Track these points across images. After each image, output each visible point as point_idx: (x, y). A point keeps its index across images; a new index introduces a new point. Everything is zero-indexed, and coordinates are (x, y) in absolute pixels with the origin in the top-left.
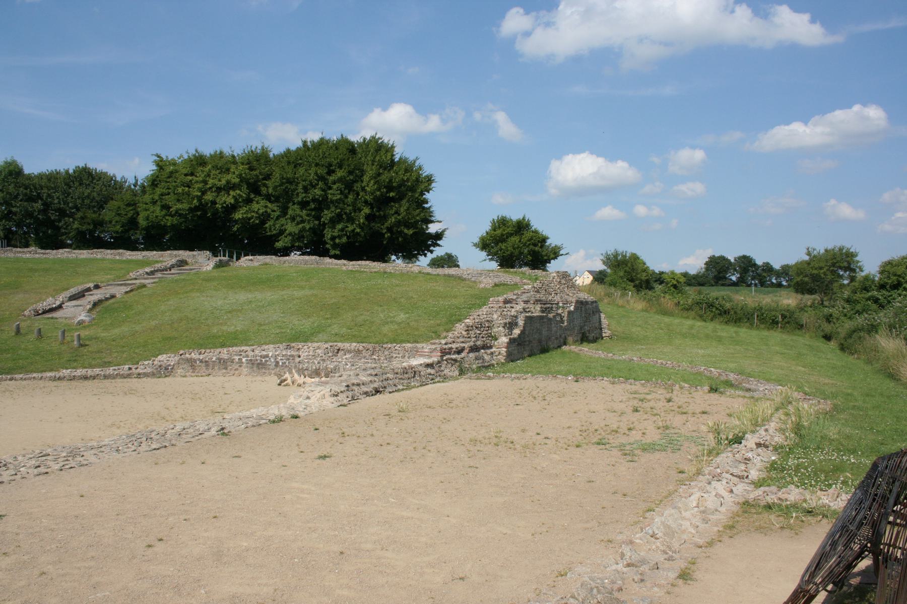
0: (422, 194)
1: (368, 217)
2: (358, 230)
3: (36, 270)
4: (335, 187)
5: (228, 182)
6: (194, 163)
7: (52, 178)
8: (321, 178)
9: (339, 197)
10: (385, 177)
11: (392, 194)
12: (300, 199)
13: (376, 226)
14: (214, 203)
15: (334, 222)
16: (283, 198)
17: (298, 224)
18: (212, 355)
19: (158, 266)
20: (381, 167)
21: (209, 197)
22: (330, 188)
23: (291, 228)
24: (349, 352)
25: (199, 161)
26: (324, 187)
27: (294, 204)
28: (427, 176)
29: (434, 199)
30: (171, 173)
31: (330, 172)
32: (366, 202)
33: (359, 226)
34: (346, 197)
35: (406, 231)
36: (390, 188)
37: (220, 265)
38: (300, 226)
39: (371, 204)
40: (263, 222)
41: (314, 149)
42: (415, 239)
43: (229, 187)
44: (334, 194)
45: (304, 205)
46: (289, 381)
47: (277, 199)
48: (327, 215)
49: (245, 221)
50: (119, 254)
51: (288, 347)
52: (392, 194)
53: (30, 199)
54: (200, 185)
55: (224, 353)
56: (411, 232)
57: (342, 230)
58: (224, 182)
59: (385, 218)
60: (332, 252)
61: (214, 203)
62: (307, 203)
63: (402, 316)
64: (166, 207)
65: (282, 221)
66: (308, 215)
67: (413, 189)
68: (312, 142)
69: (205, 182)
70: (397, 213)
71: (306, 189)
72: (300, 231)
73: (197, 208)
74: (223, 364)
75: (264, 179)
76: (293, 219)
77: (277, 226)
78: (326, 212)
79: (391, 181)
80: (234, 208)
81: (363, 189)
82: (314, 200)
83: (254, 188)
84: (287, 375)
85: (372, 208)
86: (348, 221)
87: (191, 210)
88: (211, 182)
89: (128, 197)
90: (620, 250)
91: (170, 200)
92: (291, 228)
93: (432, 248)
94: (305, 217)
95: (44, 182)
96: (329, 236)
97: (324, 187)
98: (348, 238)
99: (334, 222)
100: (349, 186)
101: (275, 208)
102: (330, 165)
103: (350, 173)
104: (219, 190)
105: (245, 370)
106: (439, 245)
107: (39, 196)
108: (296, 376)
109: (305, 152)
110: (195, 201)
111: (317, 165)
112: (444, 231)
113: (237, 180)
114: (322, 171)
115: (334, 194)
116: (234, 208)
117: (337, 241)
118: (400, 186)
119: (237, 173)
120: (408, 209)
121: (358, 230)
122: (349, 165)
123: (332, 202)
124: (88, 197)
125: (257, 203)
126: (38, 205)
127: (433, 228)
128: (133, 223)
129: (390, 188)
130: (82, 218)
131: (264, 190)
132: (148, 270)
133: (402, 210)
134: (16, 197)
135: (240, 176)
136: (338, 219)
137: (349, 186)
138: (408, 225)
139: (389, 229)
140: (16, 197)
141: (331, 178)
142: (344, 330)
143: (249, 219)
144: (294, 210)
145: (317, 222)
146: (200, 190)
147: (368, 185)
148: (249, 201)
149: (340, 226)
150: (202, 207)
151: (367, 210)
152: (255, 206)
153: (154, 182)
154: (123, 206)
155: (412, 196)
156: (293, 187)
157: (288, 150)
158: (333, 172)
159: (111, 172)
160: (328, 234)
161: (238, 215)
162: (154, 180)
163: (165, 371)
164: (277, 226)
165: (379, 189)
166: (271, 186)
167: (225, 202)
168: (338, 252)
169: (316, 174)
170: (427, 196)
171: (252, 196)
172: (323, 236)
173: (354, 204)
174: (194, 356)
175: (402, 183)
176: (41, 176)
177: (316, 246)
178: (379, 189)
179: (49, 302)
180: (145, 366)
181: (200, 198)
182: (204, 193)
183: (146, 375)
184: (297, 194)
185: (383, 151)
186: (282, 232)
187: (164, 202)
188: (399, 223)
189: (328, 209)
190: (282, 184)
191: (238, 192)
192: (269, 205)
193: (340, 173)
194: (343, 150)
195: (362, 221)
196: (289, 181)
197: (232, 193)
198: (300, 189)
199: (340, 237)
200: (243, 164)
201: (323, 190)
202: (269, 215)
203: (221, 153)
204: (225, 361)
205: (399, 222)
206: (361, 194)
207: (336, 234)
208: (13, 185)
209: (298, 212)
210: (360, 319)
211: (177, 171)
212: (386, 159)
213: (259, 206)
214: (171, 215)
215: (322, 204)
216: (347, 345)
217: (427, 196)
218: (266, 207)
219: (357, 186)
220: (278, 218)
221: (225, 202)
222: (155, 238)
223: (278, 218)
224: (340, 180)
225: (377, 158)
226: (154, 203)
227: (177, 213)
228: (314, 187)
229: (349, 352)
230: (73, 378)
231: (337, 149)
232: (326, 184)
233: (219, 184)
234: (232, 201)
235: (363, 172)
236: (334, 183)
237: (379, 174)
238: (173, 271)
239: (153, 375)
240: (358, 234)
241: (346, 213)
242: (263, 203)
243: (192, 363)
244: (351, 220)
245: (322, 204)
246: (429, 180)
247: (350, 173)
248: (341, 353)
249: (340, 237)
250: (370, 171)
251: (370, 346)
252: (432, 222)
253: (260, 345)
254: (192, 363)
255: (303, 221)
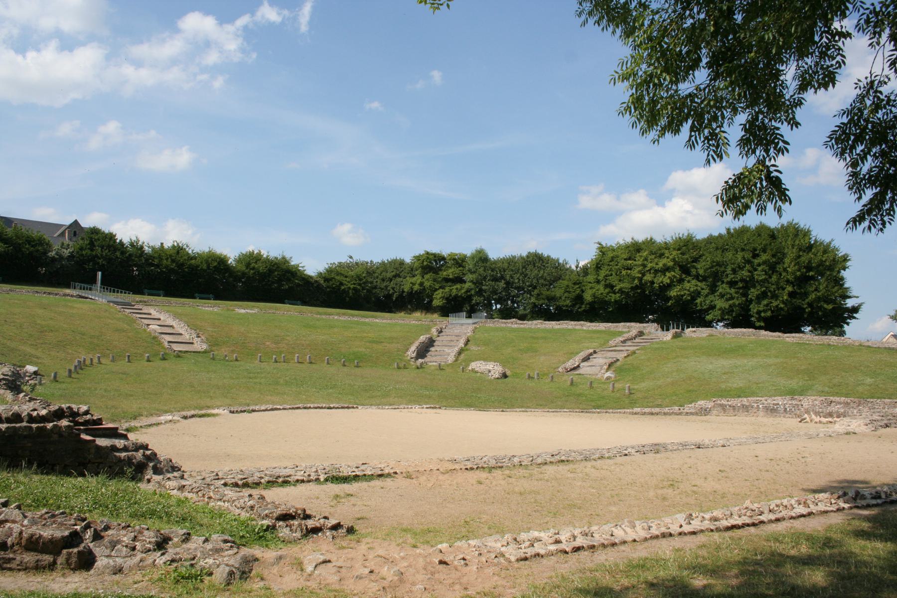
0: (839, 272)
1: (791, 295)
2: (782, 306)
3: (537, 338)
4: (760, 269)
5: (664, 265)
6: (632, 249)
7: (511, 262)
8: (748, 262)
9: (764, 277)
10: (805, 258)
11: (811, 273)
12: (729, 279)
13: (797, 302)
14: (652, 283)
15: (759, 299)
16: (714, 278)
17: (727, 300)
18: (737, 402)
19: (626, 336)
20: (800, 250)
21: (648, 277)
22: (756, 270)
23: (720, 304)
24: (840, 403)
25: (635, 248)
26: (751, 269)
27: (723, 282)
28: (843, 256)
29: (851, 277)
30: (612, 257)
31: (755, 256)
32: (788, 281)
33: (783, 302)
34: (770, 277)
35: (825, 306)
36: (809, 268)
37: (676, 336)
38: (731, 302)
39: (792, 283)
40: (693, 299)
41: (738, 236)
42: (833, 315)
43: (666, 269)
44: (759, 275)
45: (732, 284)
46: (808, 419)
47: (705, 279)
48: (753, 293)
49: (679, 298)
50: (582, 325)
51: (792, 399)
52: (811, 273)
53: (495, 279)
54: (641, 268)
55: (745, 401)
56: (830, 307)
57: (767, 305)
58: (661, 265)
59: (806, 294)
60: (758, 324)
61: (652, 283)
62: (736, 283)
63: (869, 380)
64: (611, 286)
65: (711, 297)
66: (736, 293)
67: (831, 268)
68: (735, 229)
69: (644, 266)
70: (816, 290)
71: (734, 271)
72: (730, 306)
73: (637, 287)
74: (746, 408)
75: (693, 262)
76: (722, 296)
77: (707, 302)
78: (752, 290)
79: (810, 262)
80: (669, 286)
81: (785, 270)
82: (742, 280)
83: (685, 270)
84: (806, 416)
85: (794, 286)
86: (772, 298)
87: (632, 288)
88: (649, 265)
89: (574, 278)
90: (835, 244)
91: (613, 280)
92: (720, 304)
93: (848, 321)
94: (734, 295)
95: (506, 265)
96: (755, 311)
97: (751, 269)
98: (772, 312)
99: (759, 299)
100: (773, 268)
101: (704, 287)
102: (755, 250)
103: (773, 256)
104: (656, 271)
105: (761, 413)
106: (855, 318)
107: (502, 277)
108: (813, 416)
109: (730, 238)
110: (636, 281)
111: (743, 250)
112: (860, 305)
113: (671, 264)
114: (748, 255)
115: (759, 275)
116: (669, 286)
117: (763, 314)
118: (819, 266)
119: (671, 257)
120: (827, 286)
121: (782, 306)
122: (772, 250)
123: (757, 281)
124: (542, 277)
125: (689, 282)
126: (502, 284)
127: (850, 303)
128: (579, 299)
129: (809, 268)
130: (538, 295)
131: (694, 272)
132: (621, 339)
133: (821, 287)
134: (485, 278)
135: (674, 260)
136: (764, 295)
137: (773, 268)
138: (828, 301)
139: (810, 305)
140: (485, 278)
141: (756, 261)
142: (827, 389)
143: (682, 296)
144: (723, 288)
145: (744, 299)
146: (639, 272)
147: (789, 265)
148: (681, 281)
149: (765, 302)
150: (642, 286)
151: (789, 289)
152: (687, 285)
153: (598, 265)
154: (571, 285)
155: (830, 275)
156: (722, 269)
157: (711, 235)
158: (758, 255)
159: (554, 256)
160: (754, 308)
161: (673, 293)
162: (597, 264)
163: (705, 412)
164: (707, 302)
165: (799, 270)
166: (701, 267)
167: (662, 282)
168: (762, 324)
169: (743, 258)
170: (844, 273)
171: (684, 276)
172: (750, 310)
173: (777, 283)
174: (724, 402)
175: (821, 263)
176: (503, 261)
177: (740, 319)
178: (799, 270)
179: (570, 364)
180: (688, 408)
181: (640, 279)
182: (644, 275)
183: (692, 414)
184: (727, 275)
185: (801, 236)
186: (712, 307)
187: (608, 282)
188: (818, 299)
189: (754, 287)
190: (712, 267)
191: (673, 273)
192: (699, 284)
193: (764, 257)
194: (765, 236)
195: (785, 298)
196: (719, 264)
197: (668, 274)
198: (729, 271)
199: (765, 311)
200: (674, 249)
201: (749, 271)
202: (699, 293)
203: (651, 239)
204: (747, 407)
205: (819, 297)
206: (784, 274)
207: (761, 309)
208: (482, 268)
209: (728, 290)
210: (835, 381)
211: (617, 257)
212: (804, 243)
213: (691, 285)
214: (615, 293)
215: (749, 284)
216: (837, 399)
217: (844, 273)
218: (697, 285)
219: (779, 268)
220: (707, 296)
221: (662, 282)
222: (596, 311)
223: (707, 296)
224: (764, 263)
225: (797, 242)
226: (598, 282)
227: (621, 291)
228: (741, 268)
229: (840, 403)
230: (644, 414)
231: (759, 235)
232: (752, 266)
233: (657, 267)
234: (668, 281)
235: (784, 255)
236: (759, 265)
237: (799, 257)
238: (637, 340)
239: (696, 414)
240: (781, 308)
241: (770, 291)
242: (694, 282)
243: (723, 407)
244: (775, 296)
245: (749, 284)
246: (845, 259)
247: (773, 256)
248: (833, 404)
249: (765, 311)
250: (791, 254)
251: (856, 400)
252: (850, 297)
253: (770, 396)
254: (723, 407)
255: (732, 298)
